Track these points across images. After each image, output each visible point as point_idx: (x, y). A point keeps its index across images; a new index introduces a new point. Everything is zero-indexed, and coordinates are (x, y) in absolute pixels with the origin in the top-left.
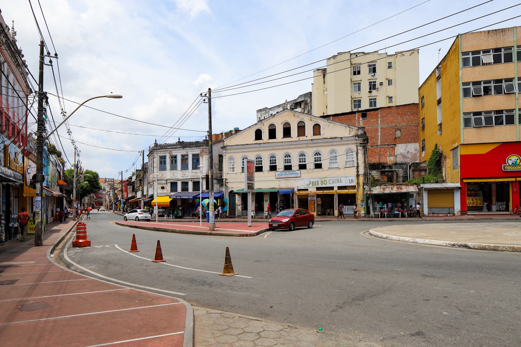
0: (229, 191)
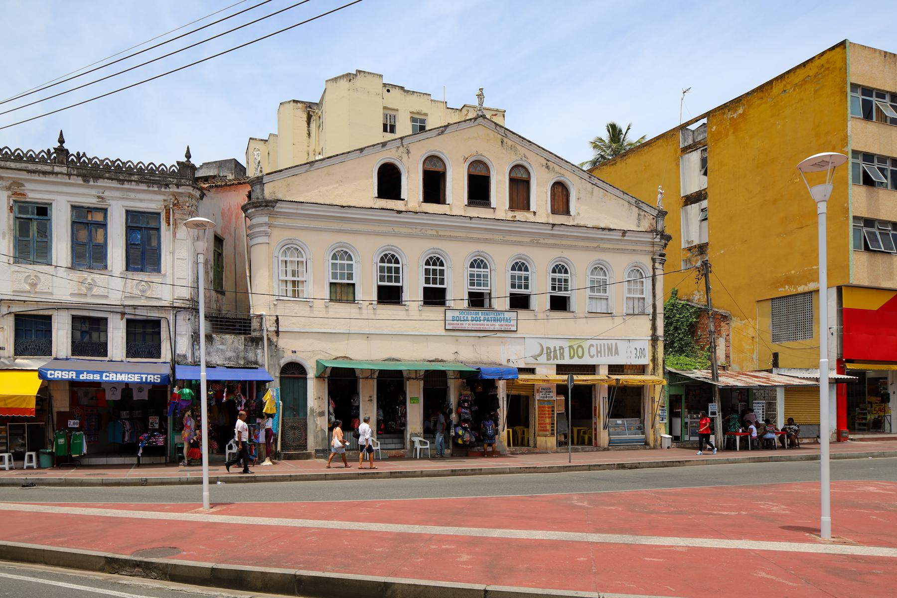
0: (283, 362)
